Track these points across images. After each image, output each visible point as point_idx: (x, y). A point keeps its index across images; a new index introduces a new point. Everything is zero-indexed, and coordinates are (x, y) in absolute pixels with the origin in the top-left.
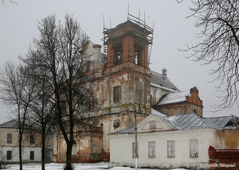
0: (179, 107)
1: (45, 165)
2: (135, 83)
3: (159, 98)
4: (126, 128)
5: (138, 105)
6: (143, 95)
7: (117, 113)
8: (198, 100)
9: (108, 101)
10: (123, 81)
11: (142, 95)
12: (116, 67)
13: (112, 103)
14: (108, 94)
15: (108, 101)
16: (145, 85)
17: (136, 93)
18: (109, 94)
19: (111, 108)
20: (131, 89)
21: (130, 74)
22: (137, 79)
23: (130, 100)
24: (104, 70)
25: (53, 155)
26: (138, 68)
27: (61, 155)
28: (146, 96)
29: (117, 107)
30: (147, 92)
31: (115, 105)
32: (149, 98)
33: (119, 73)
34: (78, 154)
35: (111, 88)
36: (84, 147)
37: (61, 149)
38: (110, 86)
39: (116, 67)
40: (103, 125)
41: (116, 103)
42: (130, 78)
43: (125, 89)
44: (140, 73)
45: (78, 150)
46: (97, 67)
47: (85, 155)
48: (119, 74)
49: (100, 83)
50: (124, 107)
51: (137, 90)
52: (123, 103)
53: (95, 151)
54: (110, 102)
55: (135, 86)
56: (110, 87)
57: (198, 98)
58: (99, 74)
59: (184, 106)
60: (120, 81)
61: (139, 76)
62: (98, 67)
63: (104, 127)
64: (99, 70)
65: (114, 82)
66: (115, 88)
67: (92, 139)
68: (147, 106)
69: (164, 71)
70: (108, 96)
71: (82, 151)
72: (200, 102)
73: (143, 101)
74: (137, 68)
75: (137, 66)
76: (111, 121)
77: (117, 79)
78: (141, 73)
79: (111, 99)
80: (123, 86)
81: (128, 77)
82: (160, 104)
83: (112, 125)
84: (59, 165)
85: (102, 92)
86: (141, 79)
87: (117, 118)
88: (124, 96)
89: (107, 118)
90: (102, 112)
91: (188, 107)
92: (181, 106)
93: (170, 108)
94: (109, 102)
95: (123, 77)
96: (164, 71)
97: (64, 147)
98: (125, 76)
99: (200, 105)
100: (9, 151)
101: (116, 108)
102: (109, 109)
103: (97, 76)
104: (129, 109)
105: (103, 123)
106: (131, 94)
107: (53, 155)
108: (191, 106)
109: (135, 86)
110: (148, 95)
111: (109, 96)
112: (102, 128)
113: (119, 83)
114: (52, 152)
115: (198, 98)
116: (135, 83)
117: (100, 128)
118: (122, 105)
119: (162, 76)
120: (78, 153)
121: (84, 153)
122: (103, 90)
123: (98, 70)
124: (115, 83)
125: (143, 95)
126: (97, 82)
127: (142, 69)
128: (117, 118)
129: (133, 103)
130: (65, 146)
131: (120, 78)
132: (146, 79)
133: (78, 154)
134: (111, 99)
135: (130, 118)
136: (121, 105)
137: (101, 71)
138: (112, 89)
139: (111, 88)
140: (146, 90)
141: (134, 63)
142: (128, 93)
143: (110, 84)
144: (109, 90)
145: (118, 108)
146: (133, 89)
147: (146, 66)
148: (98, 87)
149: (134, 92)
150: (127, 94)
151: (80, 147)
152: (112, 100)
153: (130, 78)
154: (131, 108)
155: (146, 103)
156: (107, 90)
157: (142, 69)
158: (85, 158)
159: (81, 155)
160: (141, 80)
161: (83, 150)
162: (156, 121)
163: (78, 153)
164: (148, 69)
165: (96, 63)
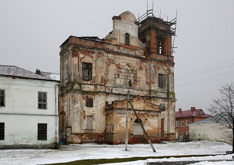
4: (87, 114)
5: (110, 92)
12: (161, 56)
25: (71, 134)
29: (162, 93)
36: (153, 127)
47: (154, 135)
48: (164, 64)
49: (144, 64)
50: (172, 95)
84: (47, 152)
87: (163, 102)
89: (156, 100)
101: (162, 93)
114: (70, 129)
121: (152, 133)
128: (163, 102)
145: (163, 94)
158: (154, 139)
161: (151, 130)
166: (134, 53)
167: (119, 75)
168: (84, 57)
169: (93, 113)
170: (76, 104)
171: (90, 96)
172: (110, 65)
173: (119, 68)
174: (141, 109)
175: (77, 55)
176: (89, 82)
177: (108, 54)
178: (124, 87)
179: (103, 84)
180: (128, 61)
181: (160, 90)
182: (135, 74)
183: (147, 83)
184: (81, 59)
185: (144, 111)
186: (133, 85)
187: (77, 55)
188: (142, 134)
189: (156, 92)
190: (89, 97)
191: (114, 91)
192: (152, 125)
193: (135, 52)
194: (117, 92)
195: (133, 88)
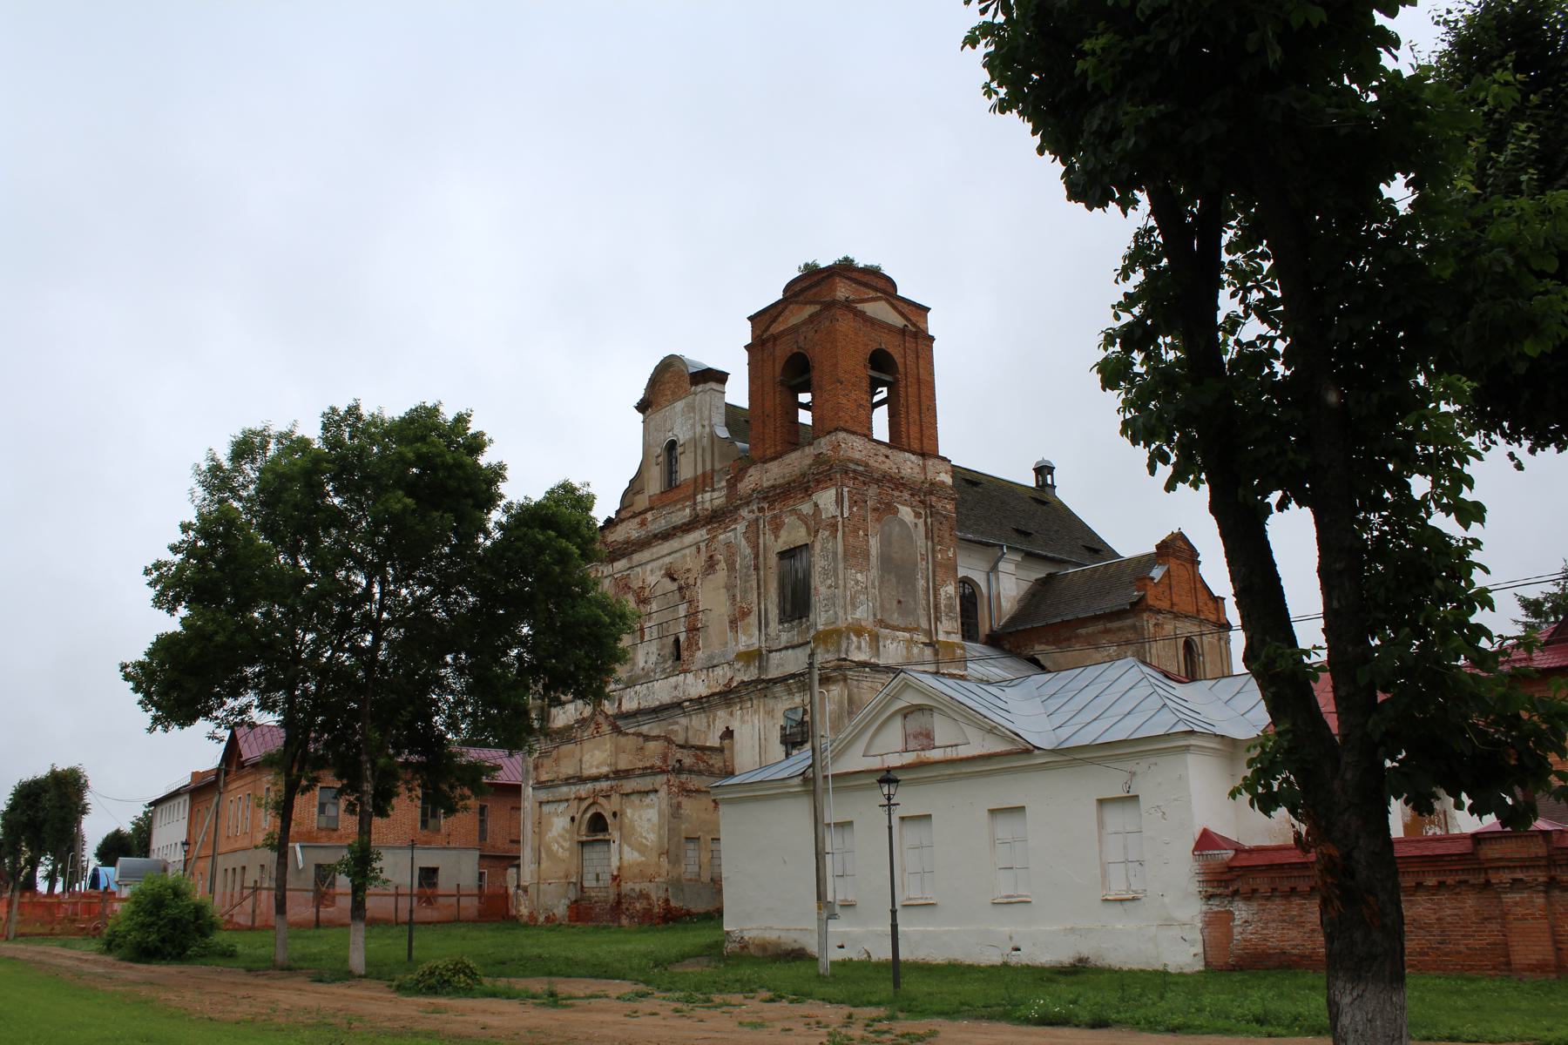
0: (1107, 631)
1: (890, 956)
2: (872, 526)
3: (1014, 593)
6: (921, 583)
7: (793, 676)
8: (1202, 598)
9: (753, 619)
10: (814, 523)
11: (914, 586)
12: (788, 461)
13: (774, 626)
14: (755, 586)
15: (753, 619)
16: (926, 538)
17: (882, 577)
18: (759, 588)
19: (770, 652)
20: (854, 555)
21: (846, 489)
22: (888, 509)
23: (855, 607)
24: (736, 476)
26: (887, 457)
27: (542, 887)
28: (934, 588)
29: (793, 647)
30: (938, 569)
31: (785, 638)
32: (950, 598)
33: (803, 486)
34: (615, 883)
35: (765, 559)
37: (543, 855)
38: (761, 546)
39: (788, 461)
40: (735, 734)
41: (792, 628)
42: (846, 504)
43: (825, 557)
44: (899, 483)
45: (615, 862)
46: (708, 467)
49: (721, 537)
51: (886, 561)
52: (821, 628)
53: (696, 869)
54: (763, 624)
55: (874, 544)
56: (761, 551)
57: (1199, 586)
58: (716, 494)
59: (1134, 627)
60: (806, 524)
61: (896, 493)
62: (713, 465)
63: (737, 747)
64: (715, 479)
65: (777, 527)
66: (787, 555)
67: (679, 805)
68: (940, 633)
69: (1043, 470)
70: (756, 595)
71: (630, 866)
72: (1211, 604)
73: (921, 612)
74: (882, 458)
75: (884, 450)
76: (770, 713)
77: (794, 512)
78: (902, 478)
79: (766, 610)
80: (818, 547)
81: (839, 501)
82: (1248, 671)
83: (776, 735)
85: (729, 577)
86: (905, 508)
87: (797, 700)
88: (822, 589)
90: (729, 675)
91: (1152, 630)
92: (1120, 629)
93: (1069, 639)
94: (757, 622)
95: (816, 505)
96: (1043, 470)
97: (555, 847)
98: (826, 499)
99: (1213, 617)
100: (428, 869)
101: (790, 651)
102: (755, 657)
103: (707, 505)
104: (847, 651)
105: (735, 725)
106: (857, 582)
107: (518, 886)
108: (1169, 628)
109: (874, 544)
110: (944, 583)
111: (759, 594)
112: (726, 752)
113: (803, 531)
114: (514, 870)
115: (1199, 586)
116: (872, 526)
117: (721, 750)
118: (818, 633)
119: (1036, 495)
120: (615, 878)
122: (731, 567)
123: (712, 479)
124: (783, 534)
125: (921, 583)
126: (708, 532)
127: (908, 465)
129: (868, 623)
130: (561, 840)
131: (806, 508)
132: (931, 506)
133: (615, 883)
134: (766, 610)
135: (856, 697)
136: (812, 633)
137: (724, 483)
138: (773, 560)
139: (765, 559)
140: (933, 558)
141: (868, 435)
142: (841, 577)
143: (761, 541)
144: (757, 568)
146: (867, 556)
147: (927, 447)
148: (711, 557)
149: (874, 573)
150: (837, 583)
151: (626, 849)
152: (774, 613)
153: (846, 504)
154: (859, 648)
155: (938, 619)
156: (748, 568)
157: (908, 465)
159: (626, 887)
160: (906, 513)
162: (931, 709)
163: (615, 878)
164: (936, 461)
165: (703, 449)
180: (667, 560)
192: (642, 837)
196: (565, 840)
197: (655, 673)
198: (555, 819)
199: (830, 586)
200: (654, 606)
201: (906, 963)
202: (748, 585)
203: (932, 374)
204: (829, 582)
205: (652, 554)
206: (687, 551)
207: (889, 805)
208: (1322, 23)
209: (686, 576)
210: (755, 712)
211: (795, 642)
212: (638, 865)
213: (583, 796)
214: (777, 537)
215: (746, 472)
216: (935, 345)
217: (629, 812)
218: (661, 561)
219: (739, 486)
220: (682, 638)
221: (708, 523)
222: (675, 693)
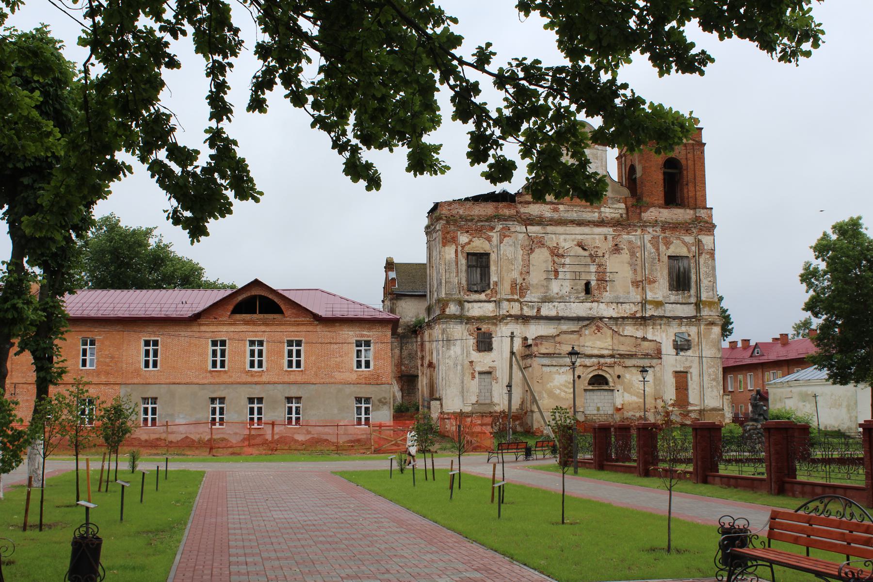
12: (675, 212)
41: (677, 295)
43: (707, 267)
65: (668, 244)
114: (438, 402)
166: (596, 215)
167: (556, 272)
168: (471, 241)
169: (492, 364)
170: (452, 348)
171: (484, 327)
172: (532, 250)
173: (558, 256)
174: (606, 352)
175: (454, 240)
176: (482, 296)
177: (528, 227)
178: (572, 300)
179: (516, 297)
180: (579, 237)
181: (673, 298)
182: (600, 266)
183: (636, 284)
184: (463, 247)
185: (612, 356)
186: (596, 292)
187: (454, 240)
188: (610, 412)
189: (658, 304)
190: (483, 330)
191: (544, 312)
193: (600, 212)
194: (553, 313)
195: (595, 299)
196: (568, 388)
197: (570, 298)
198: (557, 376)
199: (710, 281)
200: (567, 261)
201: (439, 470)
202: (654, 268)
203: (704, 190)
204: (710, 279)
205: (565, 230)
206: (597, 237)
207: (644, 381)
208: (642, 53)
209: (596, 250)
210: (663, 331)
211: (681, 302)
212: (637, 403)
213: (588, 365)
214: (668, 248)
215: (648, 209)
216: (194, 47)
217: (628, 376)
218: (573, 236)
219: (643, 214)
220: (593, 283)
221: (614, 226)
222: (589, 312)
